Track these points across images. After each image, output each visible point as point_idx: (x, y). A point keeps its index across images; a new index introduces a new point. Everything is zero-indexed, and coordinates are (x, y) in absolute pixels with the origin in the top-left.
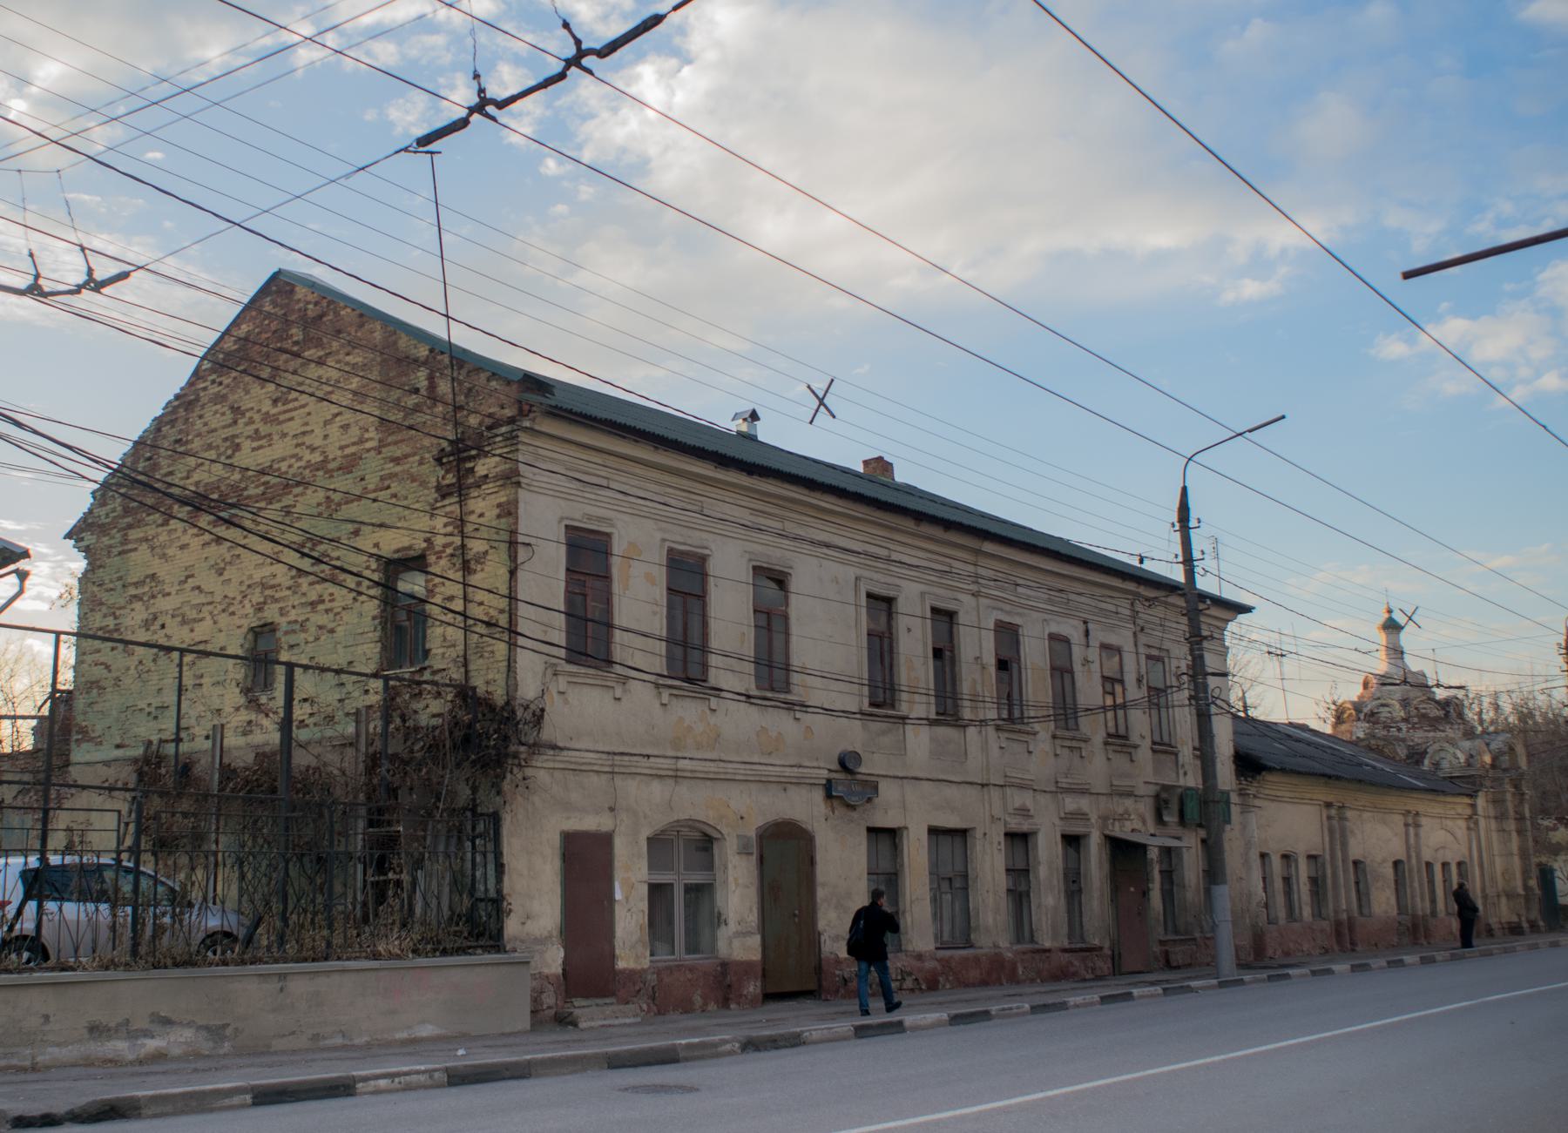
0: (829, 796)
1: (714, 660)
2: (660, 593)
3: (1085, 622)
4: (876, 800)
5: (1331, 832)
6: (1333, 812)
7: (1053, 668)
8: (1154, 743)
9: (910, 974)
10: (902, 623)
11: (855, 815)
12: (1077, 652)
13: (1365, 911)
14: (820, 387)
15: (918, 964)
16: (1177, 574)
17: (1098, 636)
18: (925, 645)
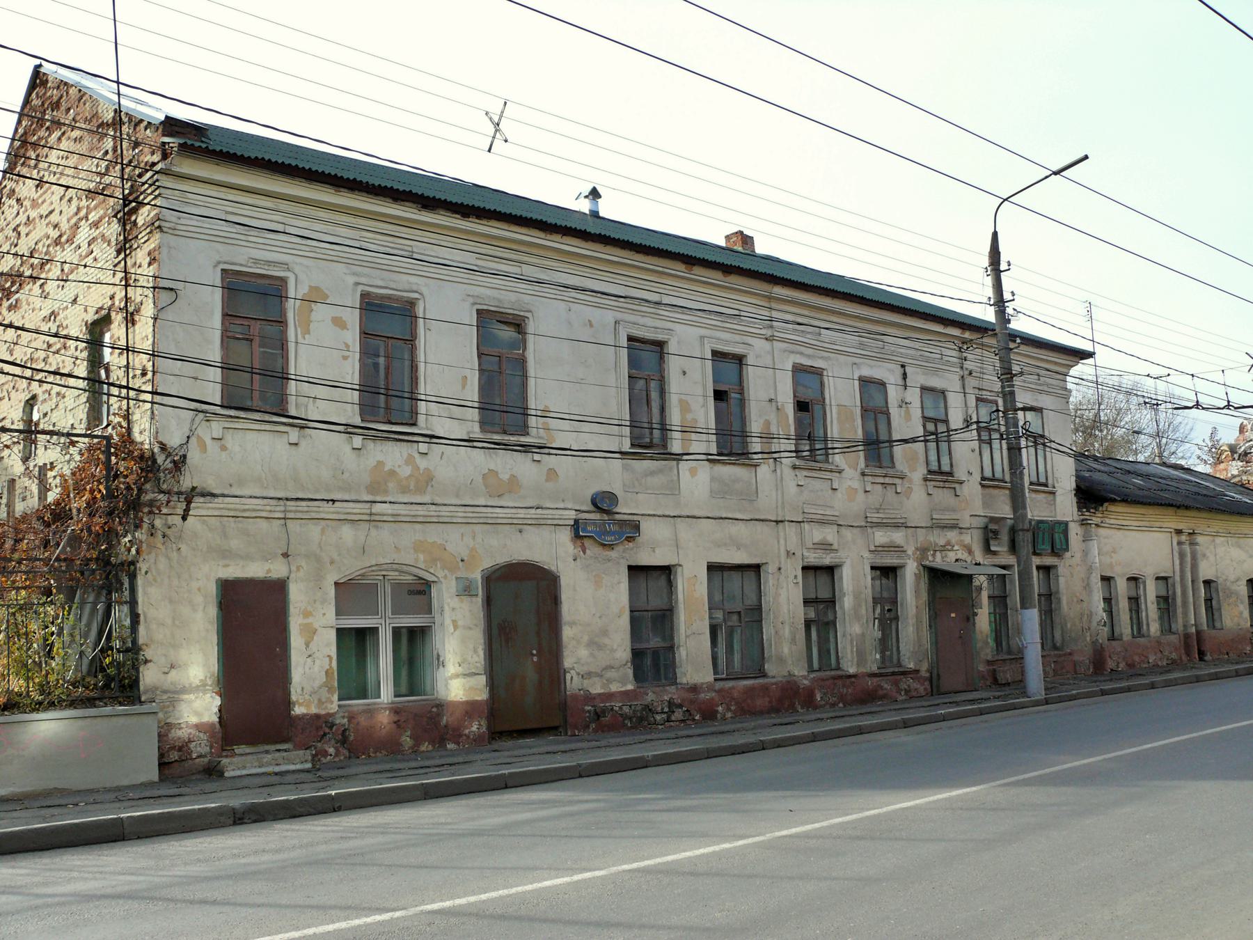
0: (577, 536)
1: (422, 406)
2: (352, 337)
3: (903, 366)
4: (639, 540)
5: (1182, 556)
6: (1183, 538)
7: (865, 410)
8: (983, 479)
9: (680, 706)
10: (674, 366)
11: (613, 554)
12: (893, 393)
13: (1218, 625)
14: (495, 109)
15: (692, 696)
16: (989, 315)
17: (917, 378)
18: (705, 387)
